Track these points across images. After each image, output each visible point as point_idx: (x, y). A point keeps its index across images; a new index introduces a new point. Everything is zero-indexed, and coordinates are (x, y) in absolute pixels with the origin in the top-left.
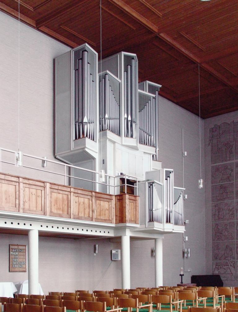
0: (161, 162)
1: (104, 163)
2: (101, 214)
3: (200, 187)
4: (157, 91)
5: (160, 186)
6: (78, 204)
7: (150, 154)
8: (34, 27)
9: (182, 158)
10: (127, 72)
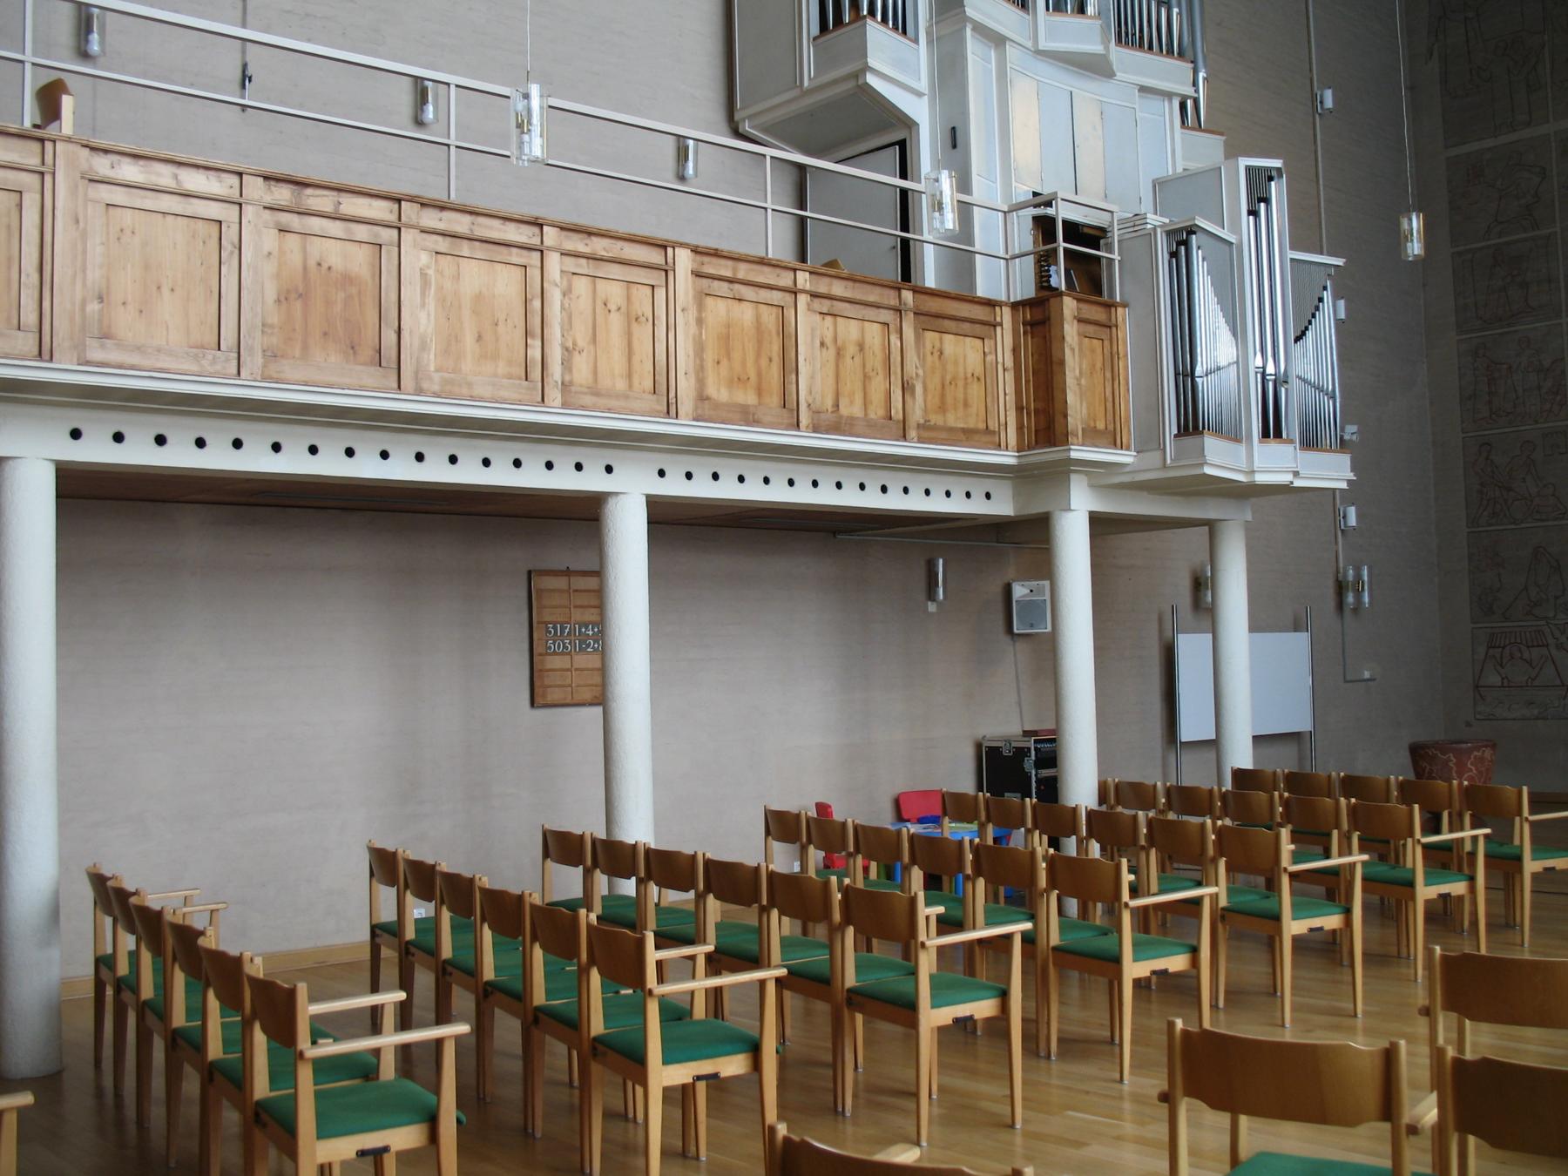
1: (954, 146)
2: (949, 400)
3: (1409, 251)
7: (1169, 95)
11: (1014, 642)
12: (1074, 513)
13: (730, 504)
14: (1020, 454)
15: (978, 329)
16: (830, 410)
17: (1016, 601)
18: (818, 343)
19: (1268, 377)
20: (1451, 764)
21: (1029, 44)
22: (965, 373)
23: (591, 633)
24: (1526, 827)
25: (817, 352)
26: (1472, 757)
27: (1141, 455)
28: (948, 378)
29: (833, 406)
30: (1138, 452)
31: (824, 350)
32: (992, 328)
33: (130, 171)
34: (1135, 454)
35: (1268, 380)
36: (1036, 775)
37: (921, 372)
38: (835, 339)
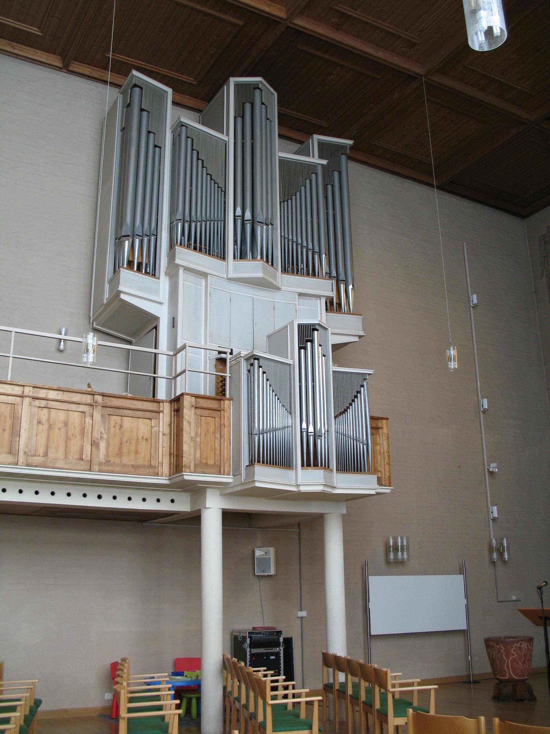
0: (361, 315)
1: (173, 327)
2: (125, 450)
4: (342, 154)
5: (288, 367)
6: (46, 426)
7: (319, 297)
8: (60, 68)
9: (470, 311)
10: (243, 117)
11: (259, 580)
12: (221, 508)
14: (170, 478)
15: (148, 414)
16: (41, 455)
17: (256, 558)
18: (35, 422)
19: (309, 434)
20: (502, 651)
21: (225, 276)
22: (137, 437)
24: (269, 710)
25: (35, 426)
26: (514, 647)
27: (235, 477)
28: (125, 439)
29: (44, 453)
30: (234, 476)
31: (40, 426)
32: (159, 413)
33: (52, 395)
34: (233, 477)
35: (310, 436)
36: (250, 652)
37: (105, 436)
38: (49, 420)
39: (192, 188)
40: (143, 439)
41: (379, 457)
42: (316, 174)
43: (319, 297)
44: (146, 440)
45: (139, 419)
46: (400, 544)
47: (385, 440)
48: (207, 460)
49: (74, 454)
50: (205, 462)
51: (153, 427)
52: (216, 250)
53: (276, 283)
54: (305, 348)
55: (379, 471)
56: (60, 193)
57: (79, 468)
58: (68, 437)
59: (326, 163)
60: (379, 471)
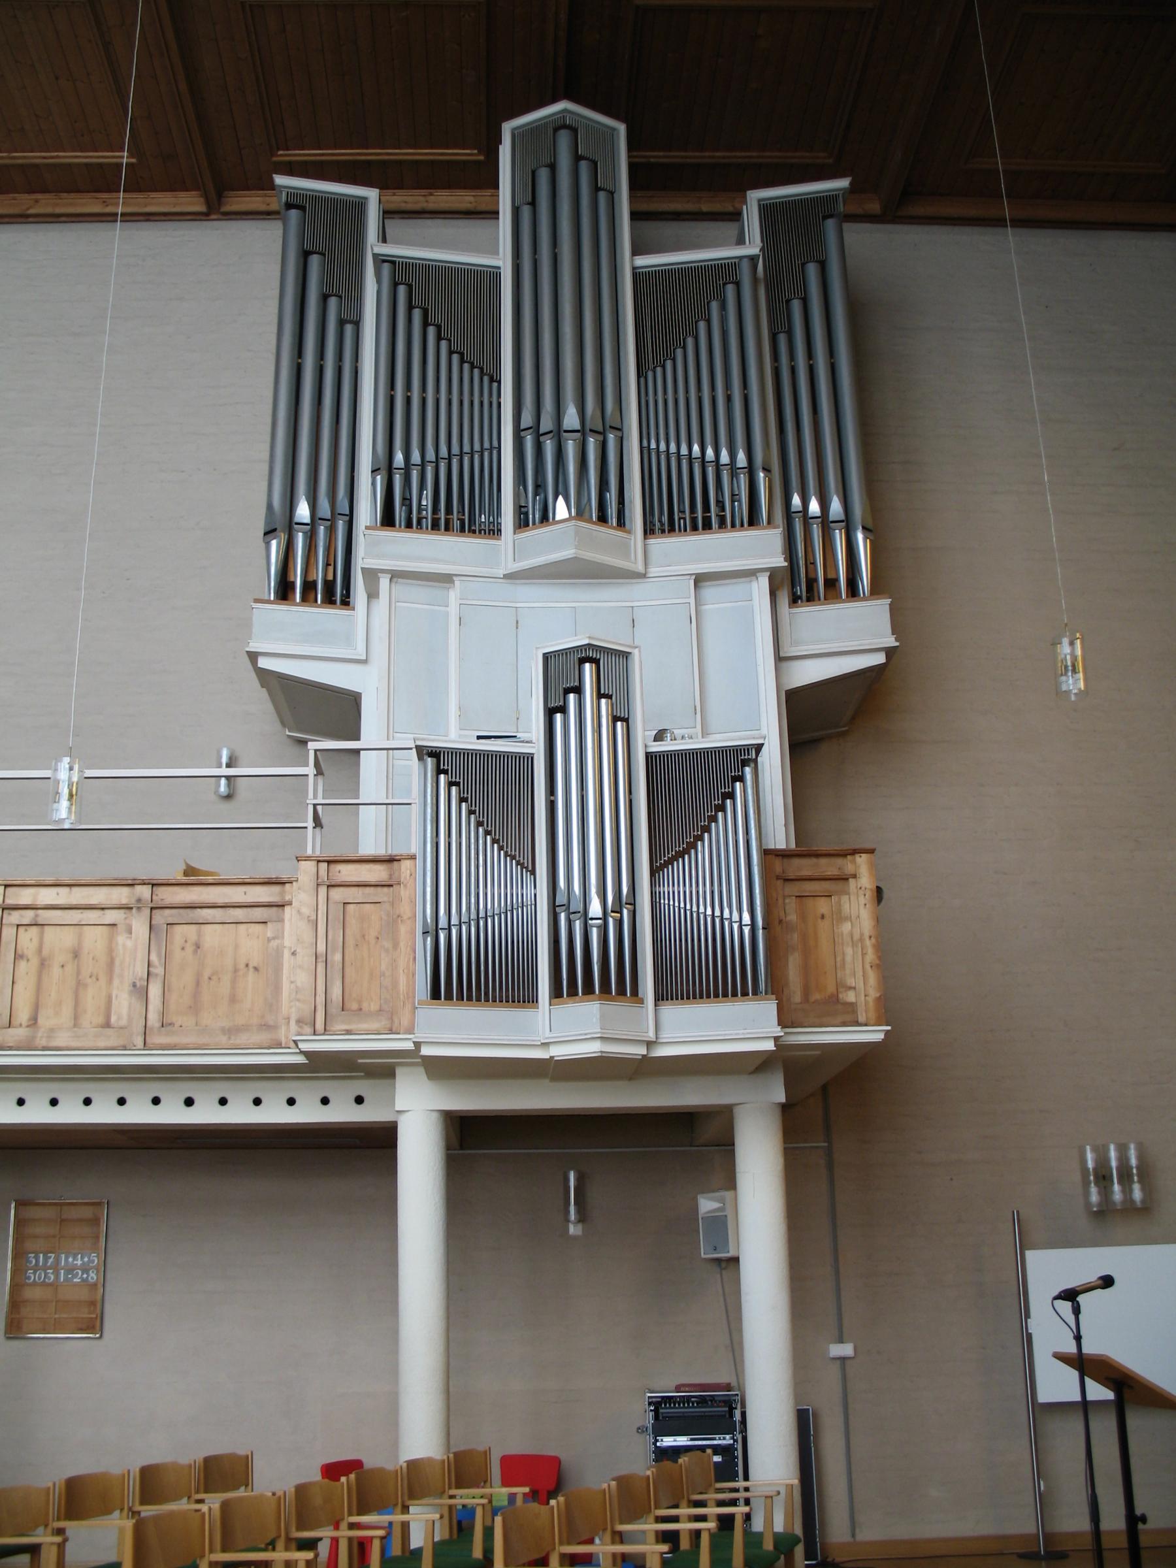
6: (35, 961)
7: (752, 573)
10: (533, 203)
13: (193, 1128)
15: (258, 913)
16: (24, 1023)
17: (702, 1218)
23: (79, 1262)
28: (207, 973)
29: (30, 1020)
33: (47, 896)
38: (40, 950)
39: (422, 395)
40: (248, 970)
41: (849, 951)
42: (738, 284)
43: (752, 573)
44: (256, 969)
45: (238, 925)
46: (1114, 1164)
47: (865, 905)
48: (360, 1002)
49: (91, 1016)
50: (355, 1006)
51: (271, 940)
52: (480, 516)
53: (630, 564)
54: (563, 710)
55: (850, 988)
56: (215, 470)
57: (102, 1044)
58: (80, 981)
59: (758, 250)
60: (850, 988)
